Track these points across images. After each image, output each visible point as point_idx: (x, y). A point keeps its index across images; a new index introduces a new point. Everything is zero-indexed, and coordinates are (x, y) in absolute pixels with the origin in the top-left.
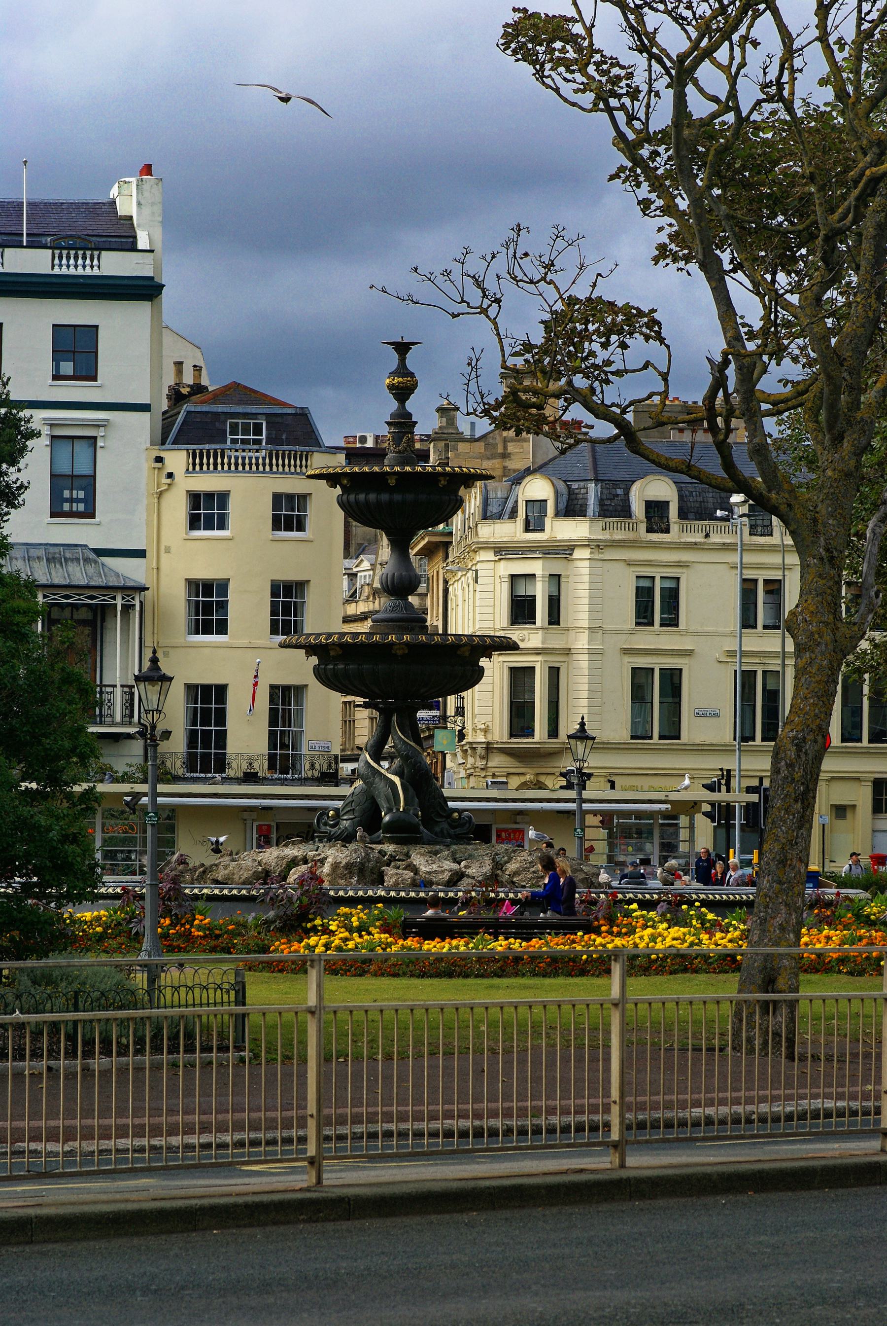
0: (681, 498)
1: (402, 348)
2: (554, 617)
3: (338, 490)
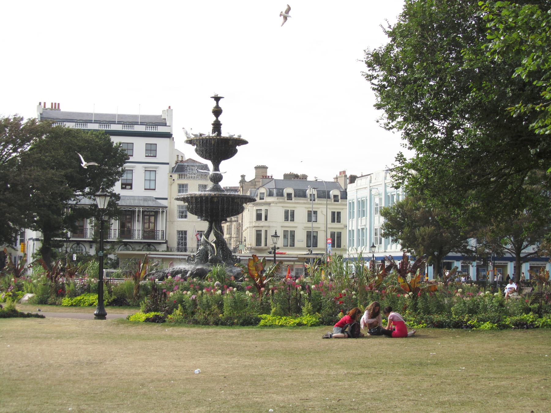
2: (266, 219)
3: (195, 147)
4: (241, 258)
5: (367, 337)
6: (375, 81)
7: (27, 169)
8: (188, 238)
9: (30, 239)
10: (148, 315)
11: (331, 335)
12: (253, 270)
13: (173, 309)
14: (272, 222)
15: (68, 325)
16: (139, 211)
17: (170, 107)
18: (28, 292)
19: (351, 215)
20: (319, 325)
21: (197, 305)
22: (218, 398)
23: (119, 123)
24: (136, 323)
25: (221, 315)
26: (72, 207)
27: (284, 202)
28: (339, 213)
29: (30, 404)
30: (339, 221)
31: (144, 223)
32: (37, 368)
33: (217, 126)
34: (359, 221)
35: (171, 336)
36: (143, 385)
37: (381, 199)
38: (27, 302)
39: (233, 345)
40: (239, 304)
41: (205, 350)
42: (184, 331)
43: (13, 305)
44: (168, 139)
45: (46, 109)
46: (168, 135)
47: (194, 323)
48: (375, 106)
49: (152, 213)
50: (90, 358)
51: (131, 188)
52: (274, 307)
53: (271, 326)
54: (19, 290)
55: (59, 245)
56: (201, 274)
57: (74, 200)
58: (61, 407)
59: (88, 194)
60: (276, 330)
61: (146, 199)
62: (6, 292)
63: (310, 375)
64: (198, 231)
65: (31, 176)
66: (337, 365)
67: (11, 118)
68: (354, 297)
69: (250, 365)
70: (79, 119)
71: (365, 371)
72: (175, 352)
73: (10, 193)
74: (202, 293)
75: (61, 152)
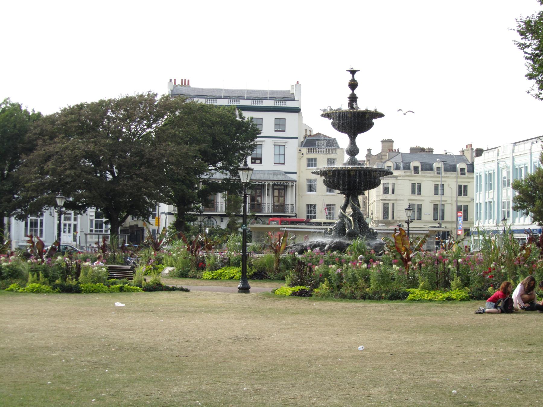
0: (422, 166)
2: (393, 193)
3: (332, 120)
4: (378, 231)
5: (520, 313)
6: (529, 50)
7: (162, 145)
8: (317, 211)
9: (162, 213)
10: (293, 288)
11: (483, 310)
12: (399, 244)
13: (319, 283)
14: (399, 195)
15: (214, 299)
16: (269, 185)
17: (298, 82)
18: (168, 266)
19: (478, 189)
20: (469, 300)
21: (342, 279)
22: (393, 377)
23: (248, 98)
24: (282, 297)
25: (368, 289)
26: (204, 182)
27: (411, 176)
28: (466, 187)
29: (202, 383)
30: (466, 194)
31: (273, 196)
32: (197, 344)
33: (353, 99)
34: (487, 194)
35: (319, 310)
36: (309, 362)
37: (508, 172)
38: (168, 275)
39: (386, 320)
40: (386, 278)
41: (360, 325)
42: (331, 305)
43: (158, 278)
44: (297, 114)
45: (177, 86)
46: (297, 110)
47: (341, 297)
48: (526, 76)
49: (282, 188)
50: (247, 333)
51: (261, 163)
52: (422, 281)
53: (420, 300)
54: (159, 264)
55: (193, 219)
56: (340, 248)
57: (207, 175)
58: (235, 386)
59: (220, 168)
60: (425, 304)
61: (275, 173)
62: (146, 266)
63: (479, 353)
64: (327, 205)
65: (166, 151)
66: (502, 341)
67: (146, 94)
68: (503, 271)
69: (413, 342)
70: (209, 95)
71: (535, 349)
72: (330, 328)
73: (146, 168)
74: (348, 266)
75: (196, 128)
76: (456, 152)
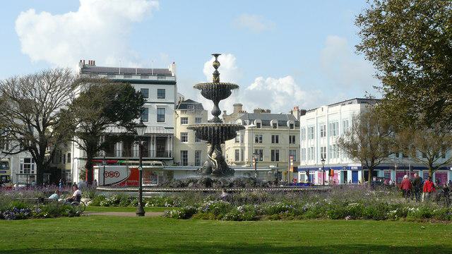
1: (216, 56)
33: (216, 75)
76: (287, 112)
